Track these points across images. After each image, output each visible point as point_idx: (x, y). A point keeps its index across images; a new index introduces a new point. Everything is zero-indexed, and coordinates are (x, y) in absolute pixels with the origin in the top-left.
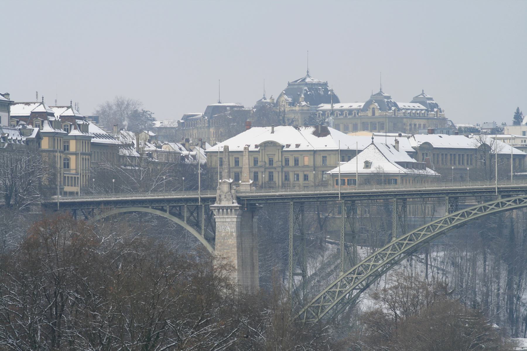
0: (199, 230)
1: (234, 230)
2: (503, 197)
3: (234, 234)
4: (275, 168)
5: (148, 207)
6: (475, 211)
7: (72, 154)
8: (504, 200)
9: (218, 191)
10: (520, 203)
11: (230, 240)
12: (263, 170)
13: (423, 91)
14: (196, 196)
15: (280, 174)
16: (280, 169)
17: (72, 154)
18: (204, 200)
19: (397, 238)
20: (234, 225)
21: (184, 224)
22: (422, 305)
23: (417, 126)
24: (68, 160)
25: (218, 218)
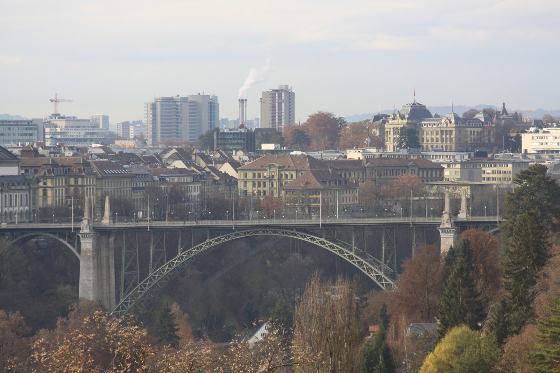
0: (74, 247)
1: (91, 247)
2: (239, 230)
3: (91, 249)
4: (275, 180)
5: (46, 232)
6: (252, 232)
7: (72, 186)
8: (239, 232)
9: (82, 224)
10: (248, 234)
11: (88, 253)
12: (268, 181)
13: (504, 104)
14: (70, 227)
15: (278, 183)
16: (277, 181)
17: (80, 186)
18: (75, 229)
19: (181, 254)
20: (91, 244)
21: (65, 243)
22: (542, 208)
23: (473, 132)
24: (78, 189)
25: (82, 241)
